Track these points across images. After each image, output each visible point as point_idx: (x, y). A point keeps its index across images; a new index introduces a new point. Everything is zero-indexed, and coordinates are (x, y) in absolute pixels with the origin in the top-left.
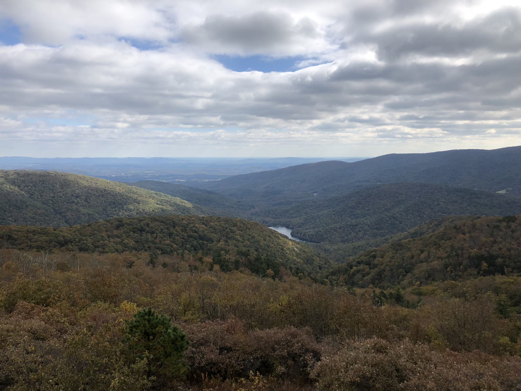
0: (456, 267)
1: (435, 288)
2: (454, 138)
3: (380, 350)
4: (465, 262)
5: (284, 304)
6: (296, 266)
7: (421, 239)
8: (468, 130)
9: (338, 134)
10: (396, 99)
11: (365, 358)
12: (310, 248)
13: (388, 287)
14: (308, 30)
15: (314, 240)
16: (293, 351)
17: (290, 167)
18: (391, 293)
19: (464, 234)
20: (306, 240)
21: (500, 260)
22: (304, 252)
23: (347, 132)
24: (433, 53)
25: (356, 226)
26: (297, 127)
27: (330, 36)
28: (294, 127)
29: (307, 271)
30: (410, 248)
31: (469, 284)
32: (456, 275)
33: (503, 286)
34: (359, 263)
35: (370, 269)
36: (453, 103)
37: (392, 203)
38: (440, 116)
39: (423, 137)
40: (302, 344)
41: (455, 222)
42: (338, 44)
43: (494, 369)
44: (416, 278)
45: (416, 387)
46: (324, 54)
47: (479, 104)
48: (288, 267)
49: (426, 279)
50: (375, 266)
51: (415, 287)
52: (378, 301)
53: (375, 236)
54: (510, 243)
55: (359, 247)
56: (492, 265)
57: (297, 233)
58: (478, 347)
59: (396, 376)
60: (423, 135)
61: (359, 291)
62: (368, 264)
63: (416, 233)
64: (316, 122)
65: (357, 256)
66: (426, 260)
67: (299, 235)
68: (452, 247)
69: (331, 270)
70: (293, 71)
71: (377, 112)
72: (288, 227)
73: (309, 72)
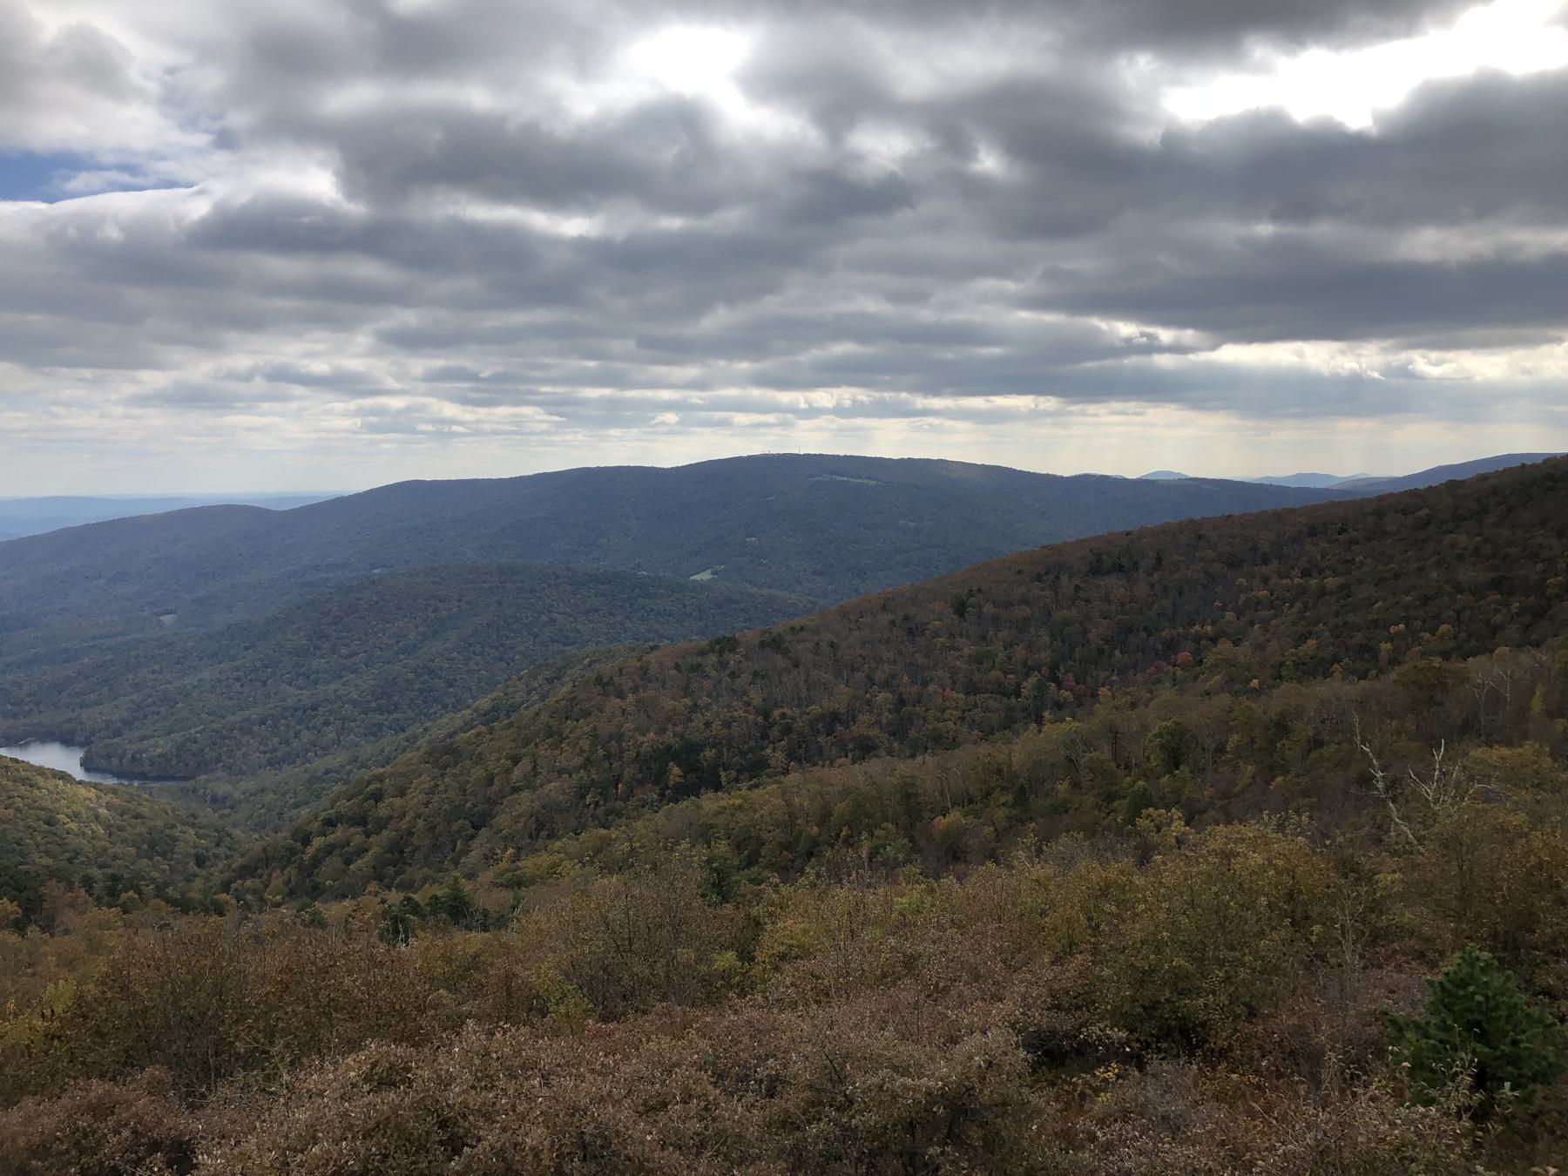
0: (606, 793)
1: (555, 858)
2: (580, 437)
3: (385, 1079)
4: (628, 773)
5: (59, 1009)
6: (110, 871)
7: (511, 725)
8: (612, 415)
9: (233, 419)
10: (408, 318)
11: (346, 1114)
12: (159, 802)
13: (425, 880)
14: (95, 68)
15: (171, 771)
16: (101, 1163)
17: (67, 532)
18: (436, 898)
19: (621, 695)
20: (144, 776)
21: (709, 753)
22: (135, 817)
23: (265, 415)
24: (501, 195)
25: (315, 708)
26: (80, 392)
27: (174, 101)
28: (67, 394)
29: (153, 880)
30: (481, 754)
31: (651, 823)
32: (608, 813)
33: (721, 820)
34: (330, 823)
35: (368, 836)
36: (567, 337)
37: (421, 629)
38: (537, 374)
39: (496, 433)
40: (135, 1132)
41: (597, 666)
42: (206, 131)
43: (704, 1044)
44: (505, 838)
45: (496, 1154)
46: (162, 158)
47: (631, 345)
48: (76, 879)
49: (531, 837)
50: (382, 825)
51: (504, 865)
52: (397, 928)
53: (375, 732)
54: (729, 706)
55: (327, 772)
56: (691, 769)
57: (108, 757)
58: (664, 998)
59: (441, 1143)
60: (495, 427)
61: (333, 910)
62: (361, 821)
63: (495, 709)
64: (152, 379)
65: (324, 802)
66: (529, 784)
67: (115, 761)
68: (594, 736)
69: (239, 861)
70: (51, 199)
71: (354, 352)
72: (67, 741)
73: (118, 208)
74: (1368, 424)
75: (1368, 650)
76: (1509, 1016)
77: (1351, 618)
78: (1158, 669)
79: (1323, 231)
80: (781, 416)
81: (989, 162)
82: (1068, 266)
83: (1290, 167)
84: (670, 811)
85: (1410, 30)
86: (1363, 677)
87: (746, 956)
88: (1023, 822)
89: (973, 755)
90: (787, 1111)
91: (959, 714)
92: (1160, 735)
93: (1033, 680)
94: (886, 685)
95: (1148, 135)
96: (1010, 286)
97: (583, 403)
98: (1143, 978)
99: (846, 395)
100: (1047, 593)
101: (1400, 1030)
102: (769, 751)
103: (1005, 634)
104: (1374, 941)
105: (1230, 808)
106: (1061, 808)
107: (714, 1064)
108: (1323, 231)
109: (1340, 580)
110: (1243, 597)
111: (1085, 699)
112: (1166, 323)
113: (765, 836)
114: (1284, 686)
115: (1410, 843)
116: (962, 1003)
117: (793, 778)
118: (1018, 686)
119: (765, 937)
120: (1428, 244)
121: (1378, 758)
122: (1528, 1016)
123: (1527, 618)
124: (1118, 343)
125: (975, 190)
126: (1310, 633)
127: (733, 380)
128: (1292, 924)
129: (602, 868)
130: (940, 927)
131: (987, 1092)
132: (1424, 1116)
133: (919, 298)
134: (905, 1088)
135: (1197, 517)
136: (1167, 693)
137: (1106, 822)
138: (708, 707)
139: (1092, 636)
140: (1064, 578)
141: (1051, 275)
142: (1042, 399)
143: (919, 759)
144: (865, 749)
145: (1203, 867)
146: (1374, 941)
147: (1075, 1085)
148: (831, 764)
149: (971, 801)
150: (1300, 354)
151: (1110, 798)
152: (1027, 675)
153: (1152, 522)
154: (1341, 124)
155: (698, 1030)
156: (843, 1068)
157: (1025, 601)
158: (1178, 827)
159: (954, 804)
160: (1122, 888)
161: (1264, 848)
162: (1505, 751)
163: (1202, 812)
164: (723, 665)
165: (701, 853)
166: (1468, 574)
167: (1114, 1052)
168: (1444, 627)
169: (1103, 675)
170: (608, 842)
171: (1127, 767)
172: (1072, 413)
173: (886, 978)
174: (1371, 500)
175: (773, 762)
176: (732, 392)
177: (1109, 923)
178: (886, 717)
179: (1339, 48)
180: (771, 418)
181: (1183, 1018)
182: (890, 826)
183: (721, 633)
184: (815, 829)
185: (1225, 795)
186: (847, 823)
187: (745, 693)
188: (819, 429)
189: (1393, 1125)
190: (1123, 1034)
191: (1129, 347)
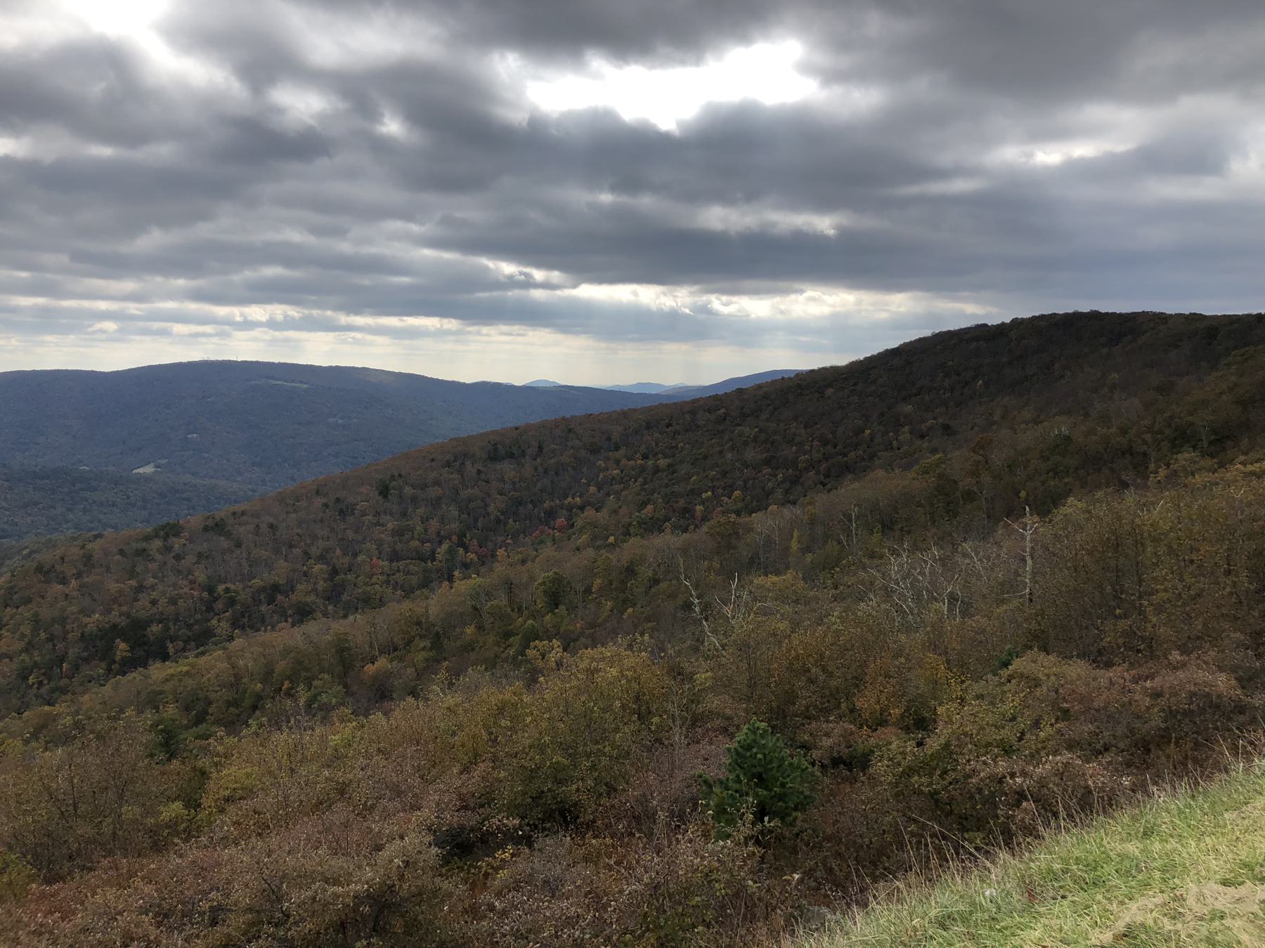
2: (13, 341)
4: (72, 652)
8: (47, 322)
19: (64, 581)
21: (155, 628)
31: (94, 698)
32: (53, 691)
33: (168, 687)
41: (37, 556)
47: (64, 259)
54: (175, 585)
58: (110, 853)
68: (36, 622)
74: (684, 347)
75: (687, 511)
76: (779, 767)
77: (676, 488)
78: (542, 532)
79: (647, 202)
80: (219, 328)
81: (392, 126)
82: (459, 215)
83: (621, 153)
84: (117, 683)
85: (698, 61)
86: (685, 531)
87: (193, 804)
88: (438, 661)
89: (398, 610)
90: (229, 935)
91: (385, 578)
92: (544, 583)
93: (445, 547)
94: (322, 558)
95: (517, 117)
96: (414, 228)
97: (15, 310)
98: (531, 775)
99: (279, 311)
100: (456, 476)
101: (711, 787)
102: (214, 622)
103: (421, 511)
104: (693, 725)
105: (596, 635)
106: (469, 647)
107: (159, 906)
108: (647, 202)
109: (668, 461)
110: (601, 476)
111: (486, 559)
112: (538, 265)
113: (212, 696)
114: (632, 540)
115: (717, 650)
116: (386, 816)
117: (238, 643)
118: (433, 552)
119: (211, 785)
120: (717, 217)
121: (696, 589)
122: (791, 764)
123: (787, 484)
124: (503, 279)
125: (382, 147)
126: (649, 500)
127: (170, 296)
128: (639, 718)
129: (47, 743)
130: (368, 756)
131: (405, 886)
132: (723, 848)
133: (339, 232)
134: (336, 896)
135: (568, 416)
136: (548, 551)
137: (504, 655)
138: (153, 588)
139: (491, 508)
140: (468, 463)
141: (446, 221)
142: (445, 321)
143: (351, 618)
144: (303, 614)
145: (574, 683)
146: (693, 725)
147: (480, 867)
148: (273, 629)
149: (395, 649)
150: (635, 294)
151: (507, 635)
152: (440, 543)
153: (535, 419)
154: (654, 125)
155: (143, 878)
156: (280, 889)
157: (437, 483)
158: (556, 653)
159: (381, 653)
160: (515, 706)
161: (617, 664)
162: (775, 579)
163: (575, 640)
164: (167, 549)
165: (149, 716)
166: (750, 454)
167: (511, 837)
168: (737, 493)
169: (500, 539)
170: (55, 718)
171: (519, 610)
172: (469, 333)
173: (320, 805)
174: (790, 379)
175: (218, 631)
176: (170, 305)
177: (504, 735)
178: (321, 585)
179: (651, 68)
180: (208, 329)
181: (561, 802)
182: (326, 676)
183: (165, 520)
184: (259, 685)
185: (593, 625)
186: (289, 678)
187: (190, 572)
188: (255, 340)
189: (703, 858)
190: (517, 822)
191: (511, 283)
